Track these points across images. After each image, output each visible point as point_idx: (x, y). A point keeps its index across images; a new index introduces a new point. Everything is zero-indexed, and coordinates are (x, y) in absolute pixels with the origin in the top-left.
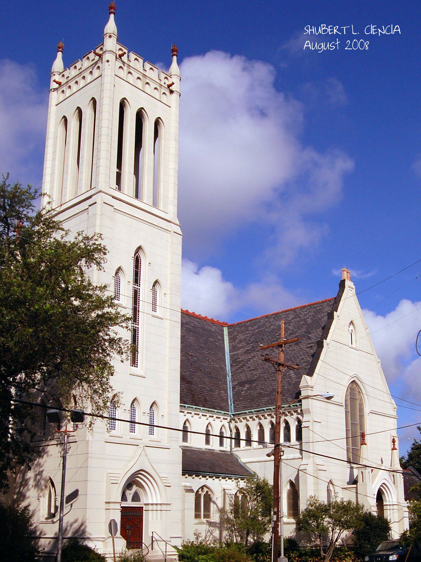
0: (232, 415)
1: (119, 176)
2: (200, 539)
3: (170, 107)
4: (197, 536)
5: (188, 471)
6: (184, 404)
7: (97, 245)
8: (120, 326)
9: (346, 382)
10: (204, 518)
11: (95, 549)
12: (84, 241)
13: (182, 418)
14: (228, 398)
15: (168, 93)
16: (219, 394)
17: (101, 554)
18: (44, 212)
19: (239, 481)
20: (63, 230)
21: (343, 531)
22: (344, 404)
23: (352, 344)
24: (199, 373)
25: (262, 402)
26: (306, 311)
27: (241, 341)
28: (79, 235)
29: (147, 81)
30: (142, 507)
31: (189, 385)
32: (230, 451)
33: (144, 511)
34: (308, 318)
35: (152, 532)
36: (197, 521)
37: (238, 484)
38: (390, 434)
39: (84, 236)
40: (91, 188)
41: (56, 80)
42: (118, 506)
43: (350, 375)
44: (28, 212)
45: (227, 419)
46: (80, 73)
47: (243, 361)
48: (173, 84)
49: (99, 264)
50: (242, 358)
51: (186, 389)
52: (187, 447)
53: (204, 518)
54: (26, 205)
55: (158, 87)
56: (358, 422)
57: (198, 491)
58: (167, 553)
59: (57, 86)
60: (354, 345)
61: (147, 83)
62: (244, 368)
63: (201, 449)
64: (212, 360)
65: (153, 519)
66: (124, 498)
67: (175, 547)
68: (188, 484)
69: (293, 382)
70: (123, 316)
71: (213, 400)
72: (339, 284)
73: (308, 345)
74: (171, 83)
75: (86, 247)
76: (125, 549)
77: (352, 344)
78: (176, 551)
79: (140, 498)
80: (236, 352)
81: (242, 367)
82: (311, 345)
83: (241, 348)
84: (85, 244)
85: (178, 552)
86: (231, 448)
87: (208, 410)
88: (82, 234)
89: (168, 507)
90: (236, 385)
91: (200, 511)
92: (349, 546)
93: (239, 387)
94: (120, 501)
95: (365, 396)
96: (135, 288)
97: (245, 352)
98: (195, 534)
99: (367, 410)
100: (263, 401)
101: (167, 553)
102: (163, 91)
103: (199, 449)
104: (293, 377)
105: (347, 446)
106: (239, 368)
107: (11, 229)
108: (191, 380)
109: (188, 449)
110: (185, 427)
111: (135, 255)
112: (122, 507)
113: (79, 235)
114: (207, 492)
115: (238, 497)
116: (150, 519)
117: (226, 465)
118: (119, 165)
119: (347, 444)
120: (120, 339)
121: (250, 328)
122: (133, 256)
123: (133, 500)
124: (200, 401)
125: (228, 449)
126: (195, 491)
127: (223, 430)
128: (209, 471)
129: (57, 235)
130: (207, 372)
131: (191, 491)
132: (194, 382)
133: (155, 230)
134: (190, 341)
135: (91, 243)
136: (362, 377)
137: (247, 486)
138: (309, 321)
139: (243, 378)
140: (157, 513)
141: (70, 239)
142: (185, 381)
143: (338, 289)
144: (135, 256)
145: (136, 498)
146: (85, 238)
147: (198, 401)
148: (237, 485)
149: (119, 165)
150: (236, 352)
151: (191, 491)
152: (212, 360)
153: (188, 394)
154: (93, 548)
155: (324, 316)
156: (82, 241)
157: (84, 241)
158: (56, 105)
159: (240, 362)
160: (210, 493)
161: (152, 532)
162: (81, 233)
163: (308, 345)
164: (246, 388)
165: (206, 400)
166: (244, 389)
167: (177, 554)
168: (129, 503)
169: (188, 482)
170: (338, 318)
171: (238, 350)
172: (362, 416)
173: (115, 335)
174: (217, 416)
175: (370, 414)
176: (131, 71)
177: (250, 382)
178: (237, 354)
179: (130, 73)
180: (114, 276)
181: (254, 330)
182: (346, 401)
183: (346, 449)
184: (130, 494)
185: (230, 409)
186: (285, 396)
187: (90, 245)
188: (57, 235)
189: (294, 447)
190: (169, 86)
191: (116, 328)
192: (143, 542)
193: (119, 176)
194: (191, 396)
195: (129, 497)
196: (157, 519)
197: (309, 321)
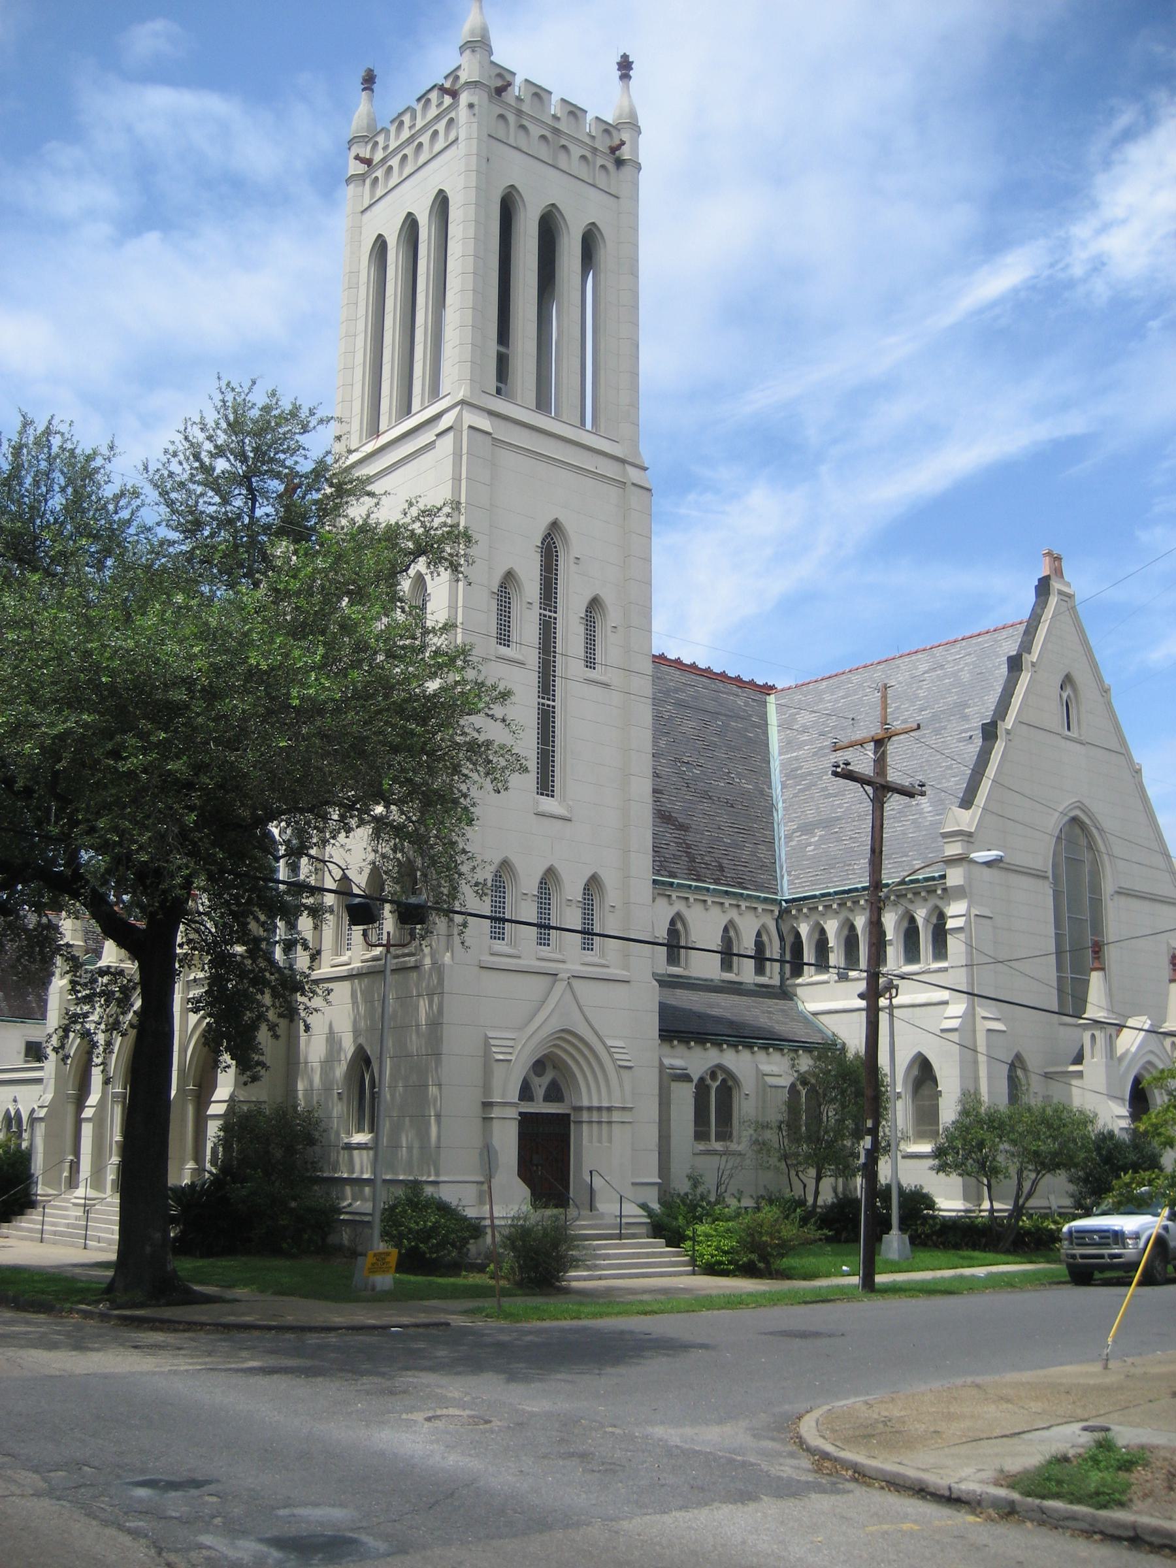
0: (783, 903)
1: (503, 362)
2: (700, 1190)
3: (617, 198)
4: (695, 1182)
5: (676, 1032)
6: (670, 877)
7: (451, 526)
8: (488, 716)
9: (1053, 822)
10: (716, 1140)
11: (458, 1206)
12: (422, 519)
13: (663, 913)
14: (775, 863)
15: (611, 166)
16: (753, 854)
17: (471, 1218)
18: (329, 460)
19: (798, 1056)
20: (371, 494)
21: (1044, 1175)
22: (1050, 874)
23: (1069, 729)
24: (706, 806)
25: (854, 869)
26: (958, 653)
27: (805, 730)
28: (411, 504)
29: (563, 142)
30: (569, 1115)
31: (683, 833)
32: (779, 984)
33: (572, 1125)
34: (962, 670)
35: (591, 1172)
36: (701, 1147)
37: (796, 1062)
38: (1168, 943)
39: (423, 509)
40: (422, 405)
41: (361, 155)
42: (513, 1113)
43: (1060, 810)
44: (296, 463)
45: (772, 911)
46: (413, 136)
47: (810, 773)
48: (623, 143)
49: (456, 567)
50: (806, 767)
51: (676, 843)
52: (678, 976)
53: (716, 1140)
54: (289, 448)
55: (588, 155)
56: (1087, 916)
57: (702, 1079)
58: (624, 1220)
59: (361, 168)
60: (1074, 734)
61: (564, 147)
62: (814, 790)
63: (712, 980)
64: (738, 774)
65: (591, 1141)
66: (526, 1093)
67: (644, 1206)
68: (678, 1062)
69: (928, 823)
70: (494, 687)
71: (739, 868)
72: (1036, 587)
73: (963, 735)
74: (618, 142)
75: (427, 531)
76: (526, 1207)
77: (1069, 729)
78: (645, 1214)
79: (562, 1094)
80: (795, 754)
81: (808, 788)
82: (969, 734)
83: (805, 743)
84: (423, 525)
85: (649, 1216)
86: (782, 979)
87: (726, 892)
88: (417, 502)
89: (627, 1117)
90: (795, 831)
91: (708, 1124)
92: (1063, 1210)
93: (800, 836)
94: (516, 1100)
95: (1106, 857)
96: (545, 616)
97: (815, 754)
98: (689, 1177)
99: (1108, 886)
100: (855, 867)
101: (624, 1220)
102: (600, 161)
103: (706, 980)
104: (926, 810)
105: (1058, 971)
106: (801, 791)
107: (261, 501)
108: (687, 821)
109: (681, 980)
110: (673, 932)
111: (544, 540)
112: (521, 1114)
113: (411, 504)
114: (724, 1081)
115: (799, 1092)
116: (585, 1142)
117: (770, 1019)
118: (504, 334)
119: (1060, 967)
120: (487, 745)
121: (827, 697)
122: (540, 545)
123: (548, 1098)
124: (709, 869)
125: (776, 981)
126: (696, 1078)
127: (765, 938)
128: (729, 1032)
129: (357, 510)
130: (727, 803)
131: (687, 1078)
132: (693, 826)
133: (590, 482)
134: (684, 729)
135: (437, 522)
136: (1096, 808)
137: (816, 1067)
138: (965, 676)
139: (811, 814)
140: (600, 1130)
141: (388, 514)
142: (674, 825)
143: (1034, 599)
144: (542, 543)
145: (554, 1093)
146: (423, 512)
147: (703, 870)
148: (793, 1066)
149: (504, 334)
150: (795, 754)
151: (687, 1078)
152: (738, 774)
153: (680, 853)
154: (454, 1203)
155: (1000, 665)
156: (417, 518)
157: (422, 519)
158: (489, 135)
159: (803, 777)
160: (730, 1083)
161: (591, 1172)
162: (414, 501)
163: (963, 735)
164: (817, 838)
165: (721, 868)
166: (812, 840)
167: (649, 1221)
168: (540, 1107)
169: (677, 1057)
170: (1034, 669)
171: (800, 748)
172: (1096, 904)
173: (476, 735)
174: (748, 905)
175: (1116, 897)
176: (525, 123)
177: (827, 823)
178: (796, 759)
179: (523, 127)
180: (496, 591)
181: (837, 701)
182: (1055, 866)
183: (1055, 984)
184: (540, 1086)
185: (779, 887)
186: (907, 856)
187: (435, 526)
188: (357, 510)
189: (914, 977)
190: (614, 150)
191: (477, 720)
192: (571, 1195)
193: (503, 362)
194: (687, 859)
195: (540, 1093)
196: (600, 1141)
197: (965, 676)
